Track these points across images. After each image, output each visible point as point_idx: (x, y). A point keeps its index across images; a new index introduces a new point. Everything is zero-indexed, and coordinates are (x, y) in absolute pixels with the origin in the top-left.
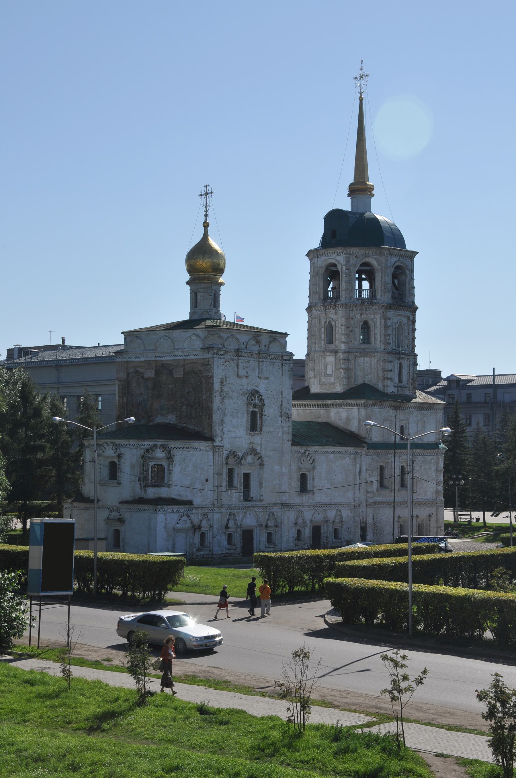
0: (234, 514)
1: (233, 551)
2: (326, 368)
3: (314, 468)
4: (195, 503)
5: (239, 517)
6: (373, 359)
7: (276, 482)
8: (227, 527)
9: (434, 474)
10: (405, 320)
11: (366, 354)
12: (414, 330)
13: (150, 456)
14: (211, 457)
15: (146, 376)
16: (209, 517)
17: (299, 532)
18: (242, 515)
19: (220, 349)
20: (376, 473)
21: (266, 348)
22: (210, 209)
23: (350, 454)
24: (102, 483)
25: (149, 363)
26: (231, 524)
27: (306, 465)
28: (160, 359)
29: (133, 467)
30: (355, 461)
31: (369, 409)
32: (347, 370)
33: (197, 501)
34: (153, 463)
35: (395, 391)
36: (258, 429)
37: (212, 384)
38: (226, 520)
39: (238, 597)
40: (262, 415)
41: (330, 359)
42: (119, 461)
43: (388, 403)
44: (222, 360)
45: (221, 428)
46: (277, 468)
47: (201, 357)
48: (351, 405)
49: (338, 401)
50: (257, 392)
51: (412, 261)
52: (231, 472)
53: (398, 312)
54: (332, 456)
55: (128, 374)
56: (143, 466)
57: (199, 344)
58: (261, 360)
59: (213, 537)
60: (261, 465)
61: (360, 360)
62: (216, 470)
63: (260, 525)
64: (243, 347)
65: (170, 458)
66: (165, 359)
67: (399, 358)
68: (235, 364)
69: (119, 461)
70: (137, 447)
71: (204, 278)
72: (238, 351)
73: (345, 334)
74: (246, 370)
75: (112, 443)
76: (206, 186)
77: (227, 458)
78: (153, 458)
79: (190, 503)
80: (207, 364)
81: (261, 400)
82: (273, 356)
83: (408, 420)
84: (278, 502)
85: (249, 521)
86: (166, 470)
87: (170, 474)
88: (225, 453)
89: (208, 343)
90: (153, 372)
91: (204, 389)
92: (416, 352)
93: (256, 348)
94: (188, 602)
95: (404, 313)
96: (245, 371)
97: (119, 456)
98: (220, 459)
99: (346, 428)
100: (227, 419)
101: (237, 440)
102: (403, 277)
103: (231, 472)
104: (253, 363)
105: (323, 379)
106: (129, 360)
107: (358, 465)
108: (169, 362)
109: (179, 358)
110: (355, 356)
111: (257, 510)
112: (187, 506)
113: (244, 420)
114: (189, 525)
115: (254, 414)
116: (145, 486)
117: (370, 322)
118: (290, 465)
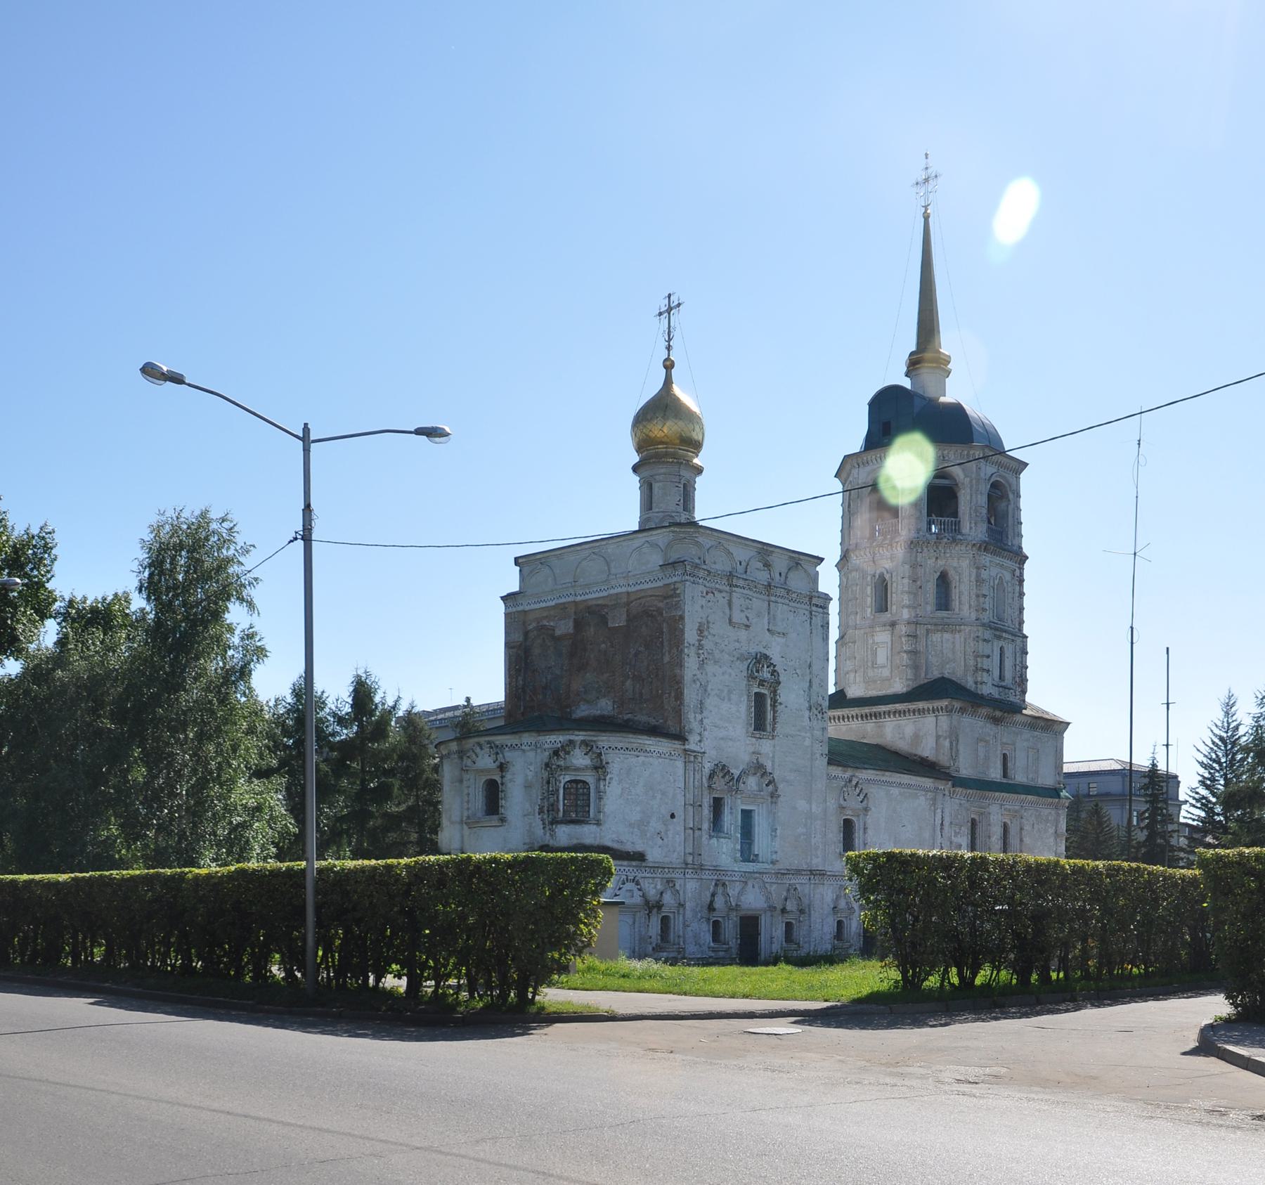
0: (724, 884)
1: (721, 954)
2: (875, 654)
3: (866, 809)
4: (649, 857)
5: (733, 891)
6: (957, 636)
7: (801, 830)
8: (711, 908)
9: (1052, 840)
10: (1008, 576)
11: (944, 626)
12: (1022, 594)
13: (562, 763)
14: (681, 771)
15: (558, 633)
16: (677, 887)
17: (840, 923)
18: (738, 886)
19: (697, 566)
20: (966, 830)
21: (783, 578)
22: (676, 335)
23: (926, 790)
24: (470, 822)
25: (563, 607)
26: (719, 903)
27: (853, 803)
28: (583, 598)
29: (528, 786)
30: (934, 804)
31: (955, 717)
32: (914, 653)
33: (654, 855)
34: (568, 778)
35: (995, 693)
36: (769, 728)
37: (682, 631)
38: (709, 895)
39: (816, 1000)
40: (774, 703)
41: (883, 637)
42: (502, 777)
43: (984, 711)
44: (701, 588)
45: (699, 717)
46: (802, 804)
47: (660, 584)
48: (921, 712)
49: (899, 706)
50: (766, 657)
51: (1018, 479)
52: (717, 805)
53: (998, 560)
54: (895, 791)
55: (526, 634)
56: (548, 783)
57: (656, 559)
58: (773, 598)
59: (685, 926)
60: (774, 795)
61: (936, 637)
62: (690, 796)
63: (772, 908)
64: (740, 569)
65: (600, 768)
66: (593, 596)
67: (999, 638)
68: (725, 601)
69: (502, 777)
70: (536, 746)
71: (666, 455)
72: (731, 575)
73: (909, 593)
74: (746, 613)
75: (489, 742)
76: (669, 296)
77: (711, 777)
78: (567, 768)
79: (640, 857)
80: (671, 595)
81: (774, 673)
82: (794, 596)
83: (1014, 744)
84: (805, 867)
85: (753, 900)
86: (592, 791)
87: (600, 798)
88: (708, 767)
89: (674, 557)
90: (571, 624)
91: (666, 643)
92: (1026, 630)
93: (763, 576)
94: (301, 669)
95: (1008, 563)
96: (743, 615)
97: (502, 767)
98: (698, 777)
99: (914, 752)
100: (710, 702)
101: (730, 743)
102: (1003, 505)
103: (717, 805)
104: (759, 603)
105: (870, 673)
106: (527, 608)
107: (939, 811)
108: (599, 602)
109: (619, 590)
110: (928, 630)
111: (766, 879)
112: (634, 863)
113: (741, 709)
114: (637, 899)
115: (759, 698)
116: (552, 823)
117: (952, 573)
118: (825, 801)
